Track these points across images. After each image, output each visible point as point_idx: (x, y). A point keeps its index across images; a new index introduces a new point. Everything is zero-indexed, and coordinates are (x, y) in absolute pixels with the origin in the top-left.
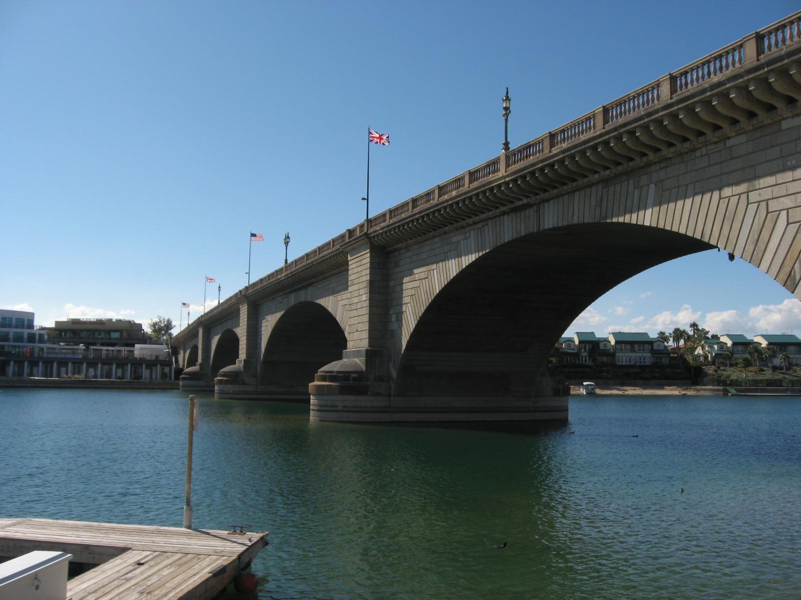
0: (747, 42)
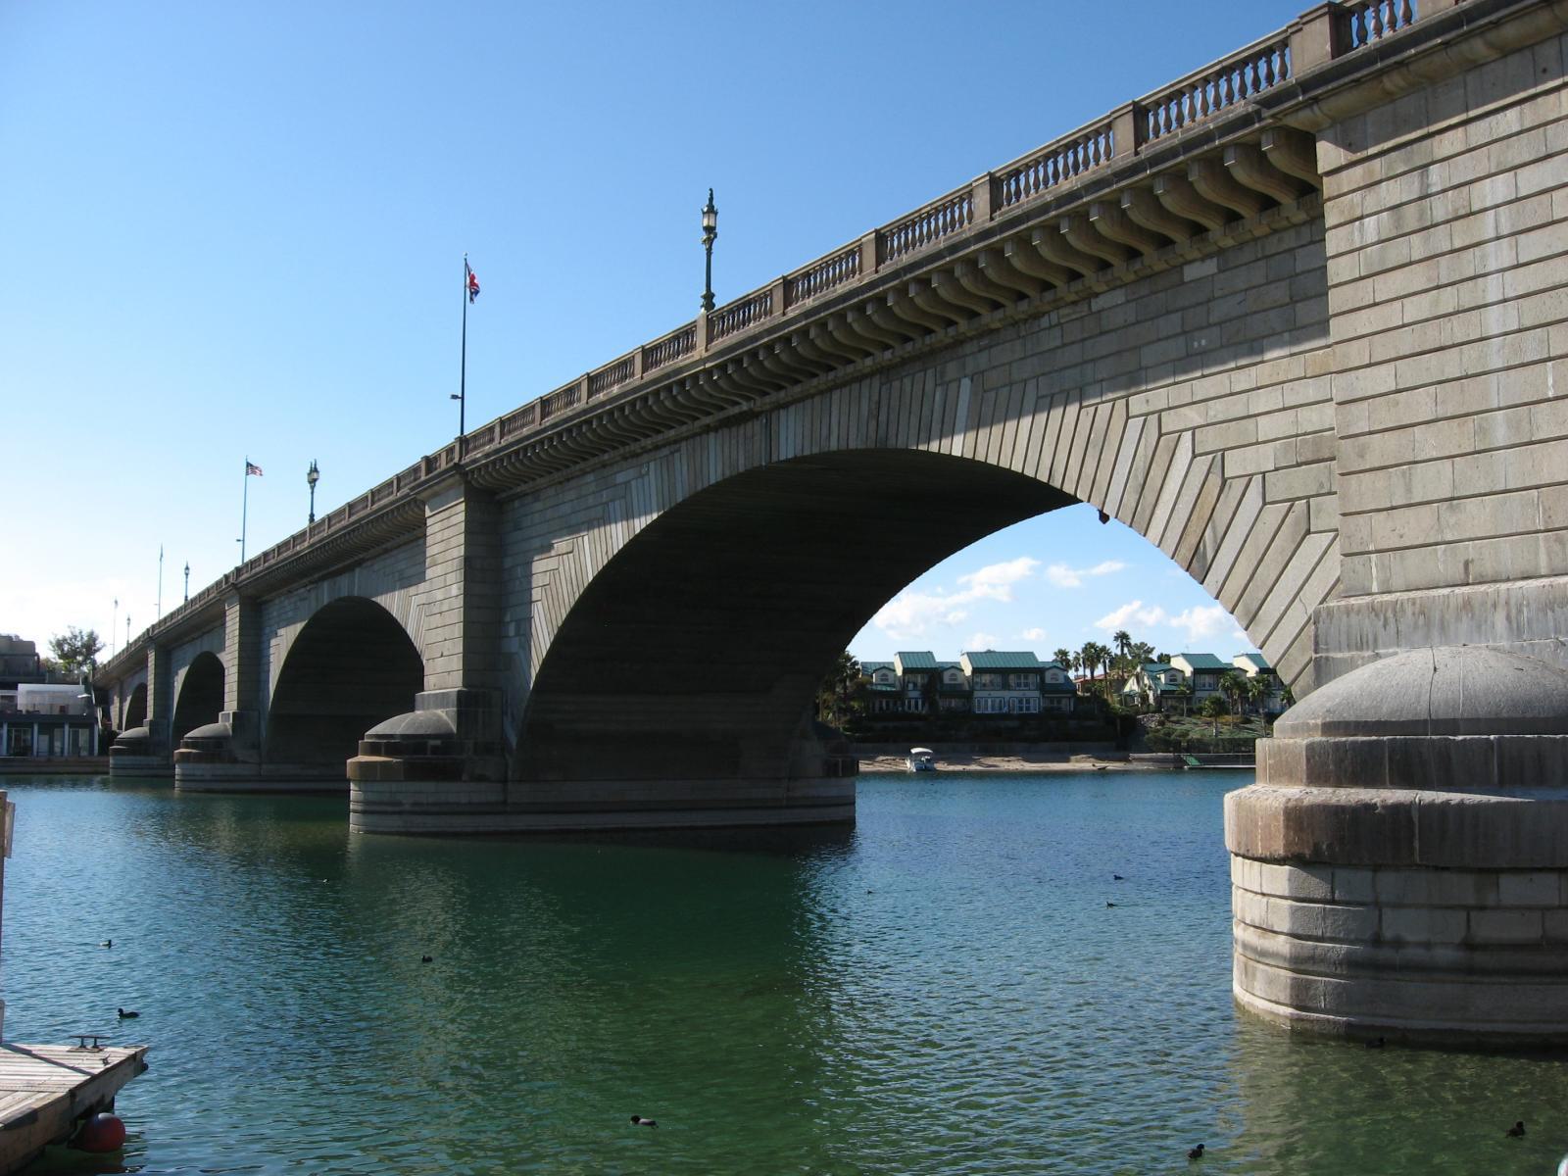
0: (1118, 120)
